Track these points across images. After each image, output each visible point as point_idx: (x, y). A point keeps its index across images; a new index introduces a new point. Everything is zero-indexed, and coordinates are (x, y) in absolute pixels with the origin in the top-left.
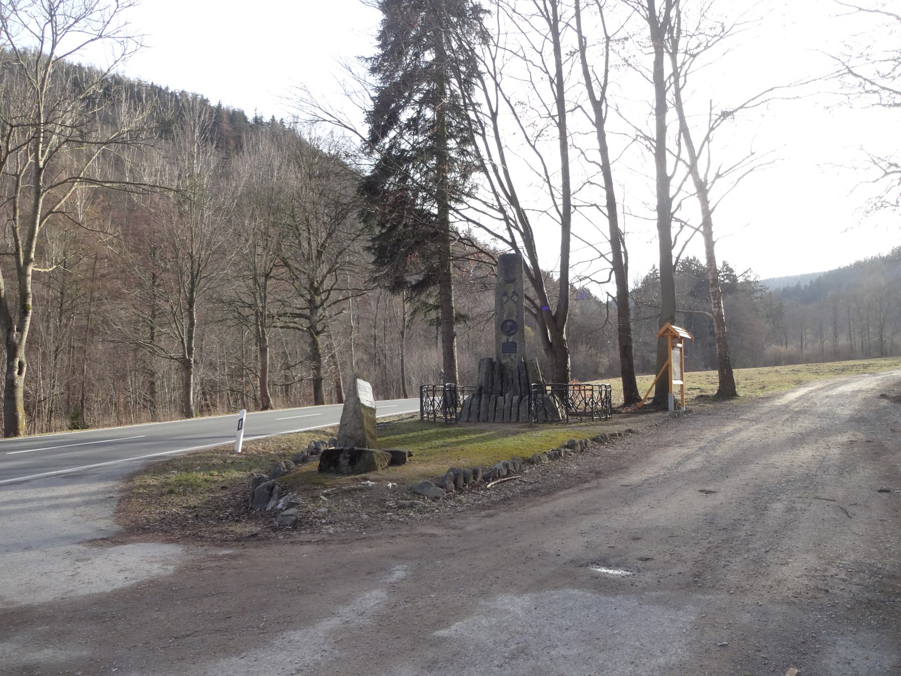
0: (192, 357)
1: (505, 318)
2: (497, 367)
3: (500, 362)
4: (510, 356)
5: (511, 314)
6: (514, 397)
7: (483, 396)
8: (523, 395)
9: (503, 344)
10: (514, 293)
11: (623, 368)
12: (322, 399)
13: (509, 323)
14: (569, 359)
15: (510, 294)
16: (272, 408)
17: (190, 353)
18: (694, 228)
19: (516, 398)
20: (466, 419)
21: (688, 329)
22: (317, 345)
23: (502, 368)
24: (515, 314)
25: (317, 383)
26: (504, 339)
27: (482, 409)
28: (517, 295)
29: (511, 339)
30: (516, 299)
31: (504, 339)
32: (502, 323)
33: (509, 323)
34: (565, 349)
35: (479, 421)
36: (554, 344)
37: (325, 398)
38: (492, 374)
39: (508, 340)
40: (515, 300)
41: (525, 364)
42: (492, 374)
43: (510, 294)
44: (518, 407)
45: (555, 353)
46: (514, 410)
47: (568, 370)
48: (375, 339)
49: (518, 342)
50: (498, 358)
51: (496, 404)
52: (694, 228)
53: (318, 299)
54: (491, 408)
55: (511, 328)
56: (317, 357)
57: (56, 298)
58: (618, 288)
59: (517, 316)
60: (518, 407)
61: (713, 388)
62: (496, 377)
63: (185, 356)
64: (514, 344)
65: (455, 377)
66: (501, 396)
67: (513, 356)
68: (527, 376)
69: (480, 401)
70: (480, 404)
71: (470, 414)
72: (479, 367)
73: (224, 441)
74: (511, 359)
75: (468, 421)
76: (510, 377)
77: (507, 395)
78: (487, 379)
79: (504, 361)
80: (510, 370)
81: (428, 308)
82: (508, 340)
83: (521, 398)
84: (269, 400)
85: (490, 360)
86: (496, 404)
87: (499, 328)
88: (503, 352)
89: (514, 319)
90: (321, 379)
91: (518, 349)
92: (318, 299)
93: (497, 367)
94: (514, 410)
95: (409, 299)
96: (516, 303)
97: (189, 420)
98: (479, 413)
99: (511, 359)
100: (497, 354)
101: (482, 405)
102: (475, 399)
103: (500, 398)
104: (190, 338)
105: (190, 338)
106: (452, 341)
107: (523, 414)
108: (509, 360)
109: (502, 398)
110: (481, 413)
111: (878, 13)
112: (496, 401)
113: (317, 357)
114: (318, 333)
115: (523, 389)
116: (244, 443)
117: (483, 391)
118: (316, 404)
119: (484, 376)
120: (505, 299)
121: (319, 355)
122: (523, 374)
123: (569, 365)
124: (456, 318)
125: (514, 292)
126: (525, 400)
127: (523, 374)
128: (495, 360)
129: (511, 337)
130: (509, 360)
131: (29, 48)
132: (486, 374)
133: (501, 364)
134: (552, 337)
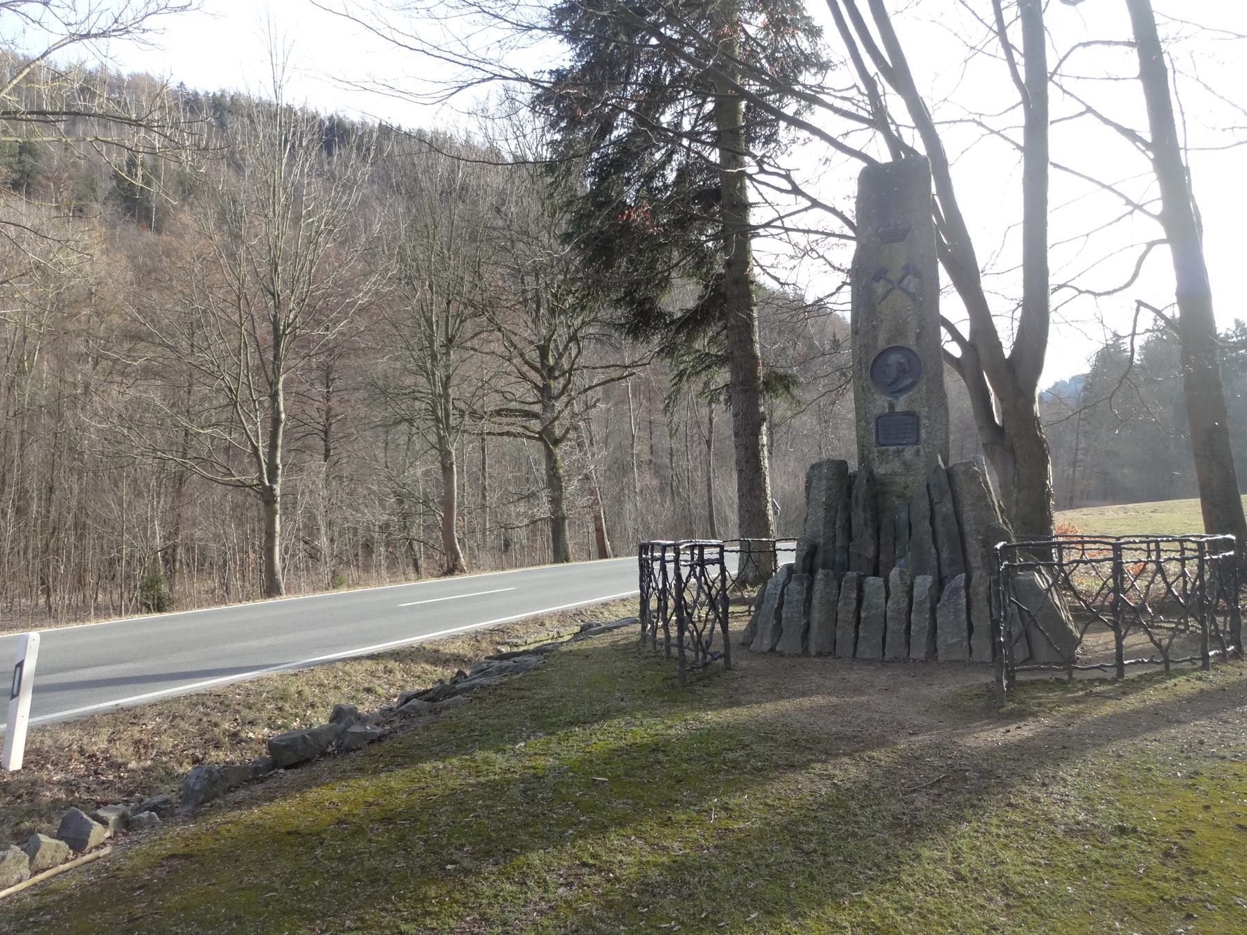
0: (276, 482)
1: (882, 344)
2: (861, 490)
3: (871, 473)
4: (899, 453)
6: (919, 580)
7: (820, 574)
8: (946, 571)
9: (879, 418)
12: (566, 551)
13: (894, 358)
14: (1050, 466)
16: (462, 571)
17: (273, 479)
19: (924, 583)
20: (766, 643)
22: (555, 461)
23: (877, 489)
25: (557, 524)
26: (881, 403)
27: (817, 616)
29: (901, 405)
31: (881, 403)
32: (873, 356)
33: (894, 358)
35: (806, 652)
37: (571, 549)
38: (847, 508)
39: (892, 406)
40: (912, 289)
41: (950, 474)
42: (847, 508)
44: (933, 611)
45: (1012, 451)
46: (919, 621)
47: (1049, 495)
48: (671, 455)
49: (924, 411)
50: (863, 459)
51: (860, 600)
53: (556, 386)
54: (846, 610)
55: (903, 371)
56: (555, 481)
58: (1179, 278)
59: (919, 336)
60: (933, 611)
62: (859, 517)
63: (263, 483)
64: (913, 416)
65: (765, 515)
66: (876, 573)
67: (909, 453)
68: (957, 514)
69: (810, 589)
70: (808, 601)
71: (778, 631)
72: (808, 488)
73: (76, 703)
74: (905, 463)
75: (772, 650)
76: (903, 515)
77: (894, 573)
78: (829, 523)
79: (881, 470)
80: (901, 496)
81: (706, 362)
82: (892, 406)
83: (940, 583)
84: (457, 557)
85: (841, 466)
86: (860, 600)
87: (866, 374)
88: (879, 444)
89: (911, 343)
90: (563, 518)
91: (923, 433)
92: (556, 386)
93: (861, 490)
94: (919, 621)
95: (668, 350)
96: (913, 297)
97: (270, 601)
98: (808, 625)
99: (905, 463)
100: (862, 447)
101: (815, 602)
102: (793, 585)
103: (873, 583)
104: (273, 447)
105: (273, 447)
106: (756, 434)
107: (949, 636)
109: (879, 581)
110: (815, 626)
111: (1097, 291)
112: (860, 590)
113: (555, 481)
114: (556, 442)
115: (945, 555)
116: (31, 729)
117: (819, 559)
118: (556, 561)
119: (821, 513)
120: (880, 287)
121: (559, 479)
122: (946, 507)
123: (1050, 482)
124: (766, 384)
126: (956, 591)
127: (946, 507)
128: (853, 466)
130: (896, 465)
131: (227, 90)
132: (828, 507)
133: (872, 479)
134: (1005, 413)
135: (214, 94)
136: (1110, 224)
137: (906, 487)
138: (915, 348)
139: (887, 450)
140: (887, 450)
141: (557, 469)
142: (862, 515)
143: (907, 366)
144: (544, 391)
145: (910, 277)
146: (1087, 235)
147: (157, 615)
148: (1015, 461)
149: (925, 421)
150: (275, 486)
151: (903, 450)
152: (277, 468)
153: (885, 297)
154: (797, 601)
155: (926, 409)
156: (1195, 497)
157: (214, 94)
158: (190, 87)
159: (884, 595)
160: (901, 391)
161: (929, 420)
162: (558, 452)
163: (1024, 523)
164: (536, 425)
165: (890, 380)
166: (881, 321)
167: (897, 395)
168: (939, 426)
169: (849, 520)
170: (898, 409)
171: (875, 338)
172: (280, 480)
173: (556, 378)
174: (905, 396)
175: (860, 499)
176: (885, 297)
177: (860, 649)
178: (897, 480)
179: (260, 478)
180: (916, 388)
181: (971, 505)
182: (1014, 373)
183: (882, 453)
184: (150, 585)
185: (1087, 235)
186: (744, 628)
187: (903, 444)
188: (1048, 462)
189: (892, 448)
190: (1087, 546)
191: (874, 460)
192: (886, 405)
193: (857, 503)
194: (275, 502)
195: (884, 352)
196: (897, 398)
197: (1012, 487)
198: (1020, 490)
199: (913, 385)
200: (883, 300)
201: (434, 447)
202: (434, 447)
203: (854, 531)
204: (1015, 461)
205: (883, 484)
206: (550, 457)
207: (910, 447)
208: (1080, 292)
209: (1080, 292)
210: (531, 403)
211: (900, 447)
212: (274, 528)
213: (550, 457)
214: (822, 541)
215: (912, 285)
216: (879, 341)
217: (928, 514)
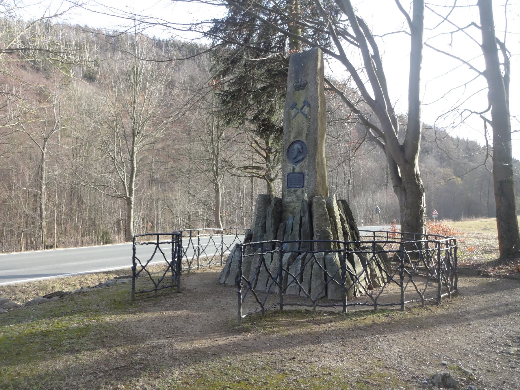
1: (292, 139)
4: (295, 191)
5: (299, 134)
10: (306, 103)
11: (498, 210)
13: (297, 146)
15: (300, 106)
17: (130, 194)
18: (447, 20)
21: (6, 127)
22: (271, 188)
24: (305, 132)
26: (290, 167)
28: (309, 106)
30: (306, 110)
33: (297, 146)
34: (418, 186)
36: (404, 180)
39: (294, 169)
40: (306, 113)
43: (300, 106)
45: (405, 190)
49: (306, 172)
52: (447, 20)
55: (299, 152)
57: (331, 134)
61: (376, 233)
78: (257, 224)
82: (294, 169)
89: (303, 139)
105: (131, 181)
108: (294, 197)
114: (272, 180)
120: (293, 112)
125: (304, 102)
129: (299, 165)
135: (166, 40)
136: (475, 79)
137: (295, 208)
138: (305, 141)
139: (291, 190)
140: (291, 190)
141: (272, 192)
142: (270, 221)
143: (301, 150)
144: (267, 158)
145: (306, 107)
146: (465, 85)
147: (97, 246)
148: (406, 195)
149: (306, 177)
150: (131, 197)
151: (297, 190)
152: (132, 190)
153: (295, 116)
154: (237, 260)
155: (307, 171)
156: (490, 216)
157: (166, 40)
158: (157, 37)
159: (270, 260)
160: (298, 162)
161: (308, 176)
162: (272, 185)
163: (408, 225)
164: (264, 173)
165: (294, 157)
166: (293, 129)
167: (297, 164)
168: (312, 179)
169: (265, 223)
170: (296, 171)
171: (290, 136)
172: (133, 195)
173: (272, 153)
174: (299, 164)
175: (270, 214)
176: (295, 116)
177: (258, 285)
178: (292, 205)
179: (126, 194)
180: (304, 161)
181: (316, 218)
182: (404, 152)
183: (289, 191)
184: (105, 233)
185: (465, 85)
186: (221, 271)
187: (297, 188)
188: (422, 195)
189: (293, 189)
190: (385, 240)
191: (286, 194)
192: (292, 168)
193: (269, 215)
194: (131, 204)
195: (293, 143)
196: (296, 165)
197: (404, 207)
198: (407, 209)
199: (303, 159)
200: (294, 118)
201: (212, 182)
202: (212, 182)
203: (267, 229)
204: (406, 195)
205: (285, 207)
206: (269, 185)
207: (300, 189)
208: (472, 112)
209: (472, 112)
210: (263, 164)
211: (296, 189)
212: (131, 214)
213: (269, 185)
214: (254, 232)
215: (306, 110)
216: (291, 138)
217: (299, 222)
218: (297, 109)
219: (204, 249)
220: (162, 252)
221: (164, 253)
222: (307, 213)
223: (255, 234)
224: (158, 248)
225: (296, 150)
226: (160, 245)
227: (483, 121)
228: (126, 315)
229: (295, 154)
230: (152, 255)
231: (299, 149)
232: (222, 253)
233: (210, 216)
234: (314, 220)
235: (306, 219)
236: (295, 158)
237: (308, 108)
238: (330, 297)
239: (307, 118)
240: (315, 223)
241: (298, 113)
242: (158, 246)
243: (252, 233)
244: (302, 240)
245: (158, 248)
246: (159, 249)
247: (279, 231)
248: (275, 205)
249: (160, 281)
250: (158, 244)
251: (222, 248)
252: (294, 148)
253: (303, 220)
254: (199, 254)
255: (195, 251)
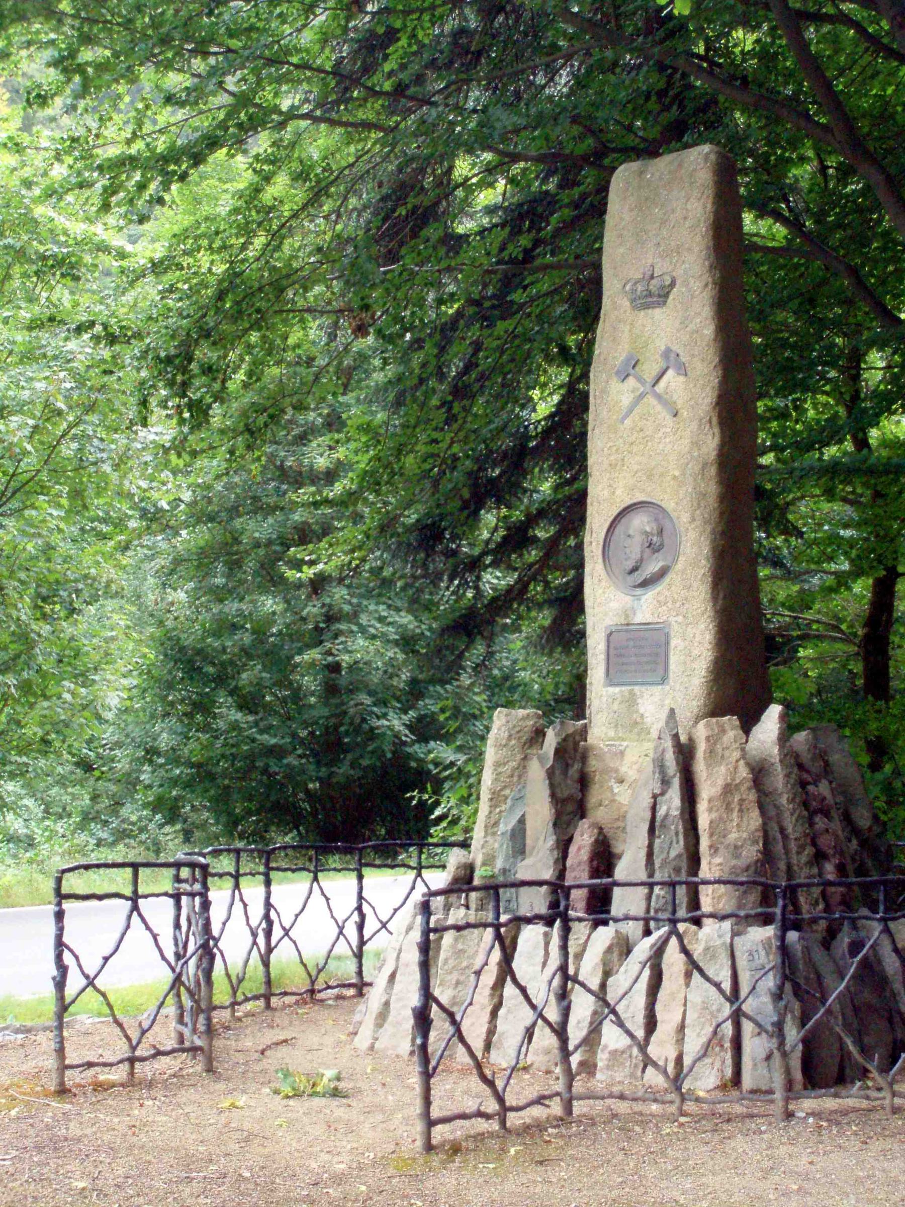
15: (650, 369)
33: (640, 522)
43: (650, 369)
125: (667, 353)
129: (649, 596)
145: (670, 373)
165: (630, 564)
167: (639, 591)
199: (662, 573)
217: (648, 815)
218: (640, 379)
219: (287, 926)
220: (148, 928)
221: (156, 931)
222: (676, 783)
223: (484, 864)
224: (135, 913)
225: (638, 539)
226: (141, 902)
227: (355, 905)
228: (800, 1055)
229: (634, 549)
230: (118, 936)
231: (646, 533)
232: (362, 943)
233: (443, 710)
234: (702, 807)
235: (673, 801)
236: (634, 570)
237: (682, 379)
238: (747, 1081)
239: (675, 415)
240: (704, 820)
241: (642, 396)
242: (135, 908)
243: (474, 860)
244: (658, 877)
245: (135, 913)
246: (140, 915)
247: (573, 849)
248: (557, 752)
249: (320, 971)
250: (135, 898)
251: (361, 927)
252: (631, 532)
253: (661, 811)
254: (270, 950)
255: (254, 935)
